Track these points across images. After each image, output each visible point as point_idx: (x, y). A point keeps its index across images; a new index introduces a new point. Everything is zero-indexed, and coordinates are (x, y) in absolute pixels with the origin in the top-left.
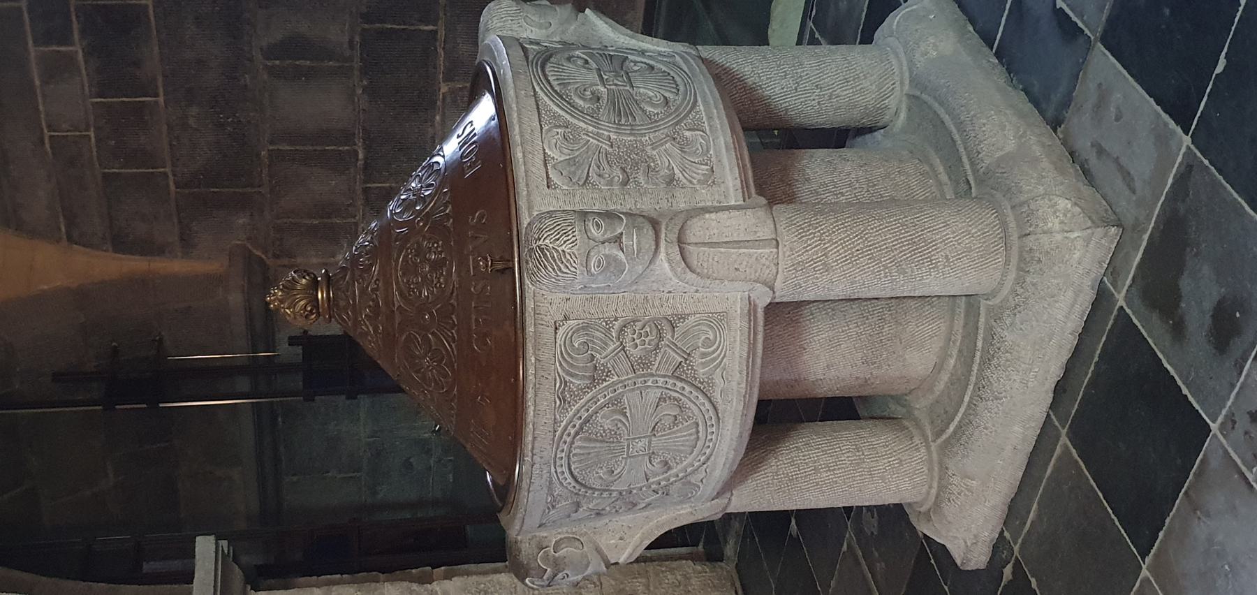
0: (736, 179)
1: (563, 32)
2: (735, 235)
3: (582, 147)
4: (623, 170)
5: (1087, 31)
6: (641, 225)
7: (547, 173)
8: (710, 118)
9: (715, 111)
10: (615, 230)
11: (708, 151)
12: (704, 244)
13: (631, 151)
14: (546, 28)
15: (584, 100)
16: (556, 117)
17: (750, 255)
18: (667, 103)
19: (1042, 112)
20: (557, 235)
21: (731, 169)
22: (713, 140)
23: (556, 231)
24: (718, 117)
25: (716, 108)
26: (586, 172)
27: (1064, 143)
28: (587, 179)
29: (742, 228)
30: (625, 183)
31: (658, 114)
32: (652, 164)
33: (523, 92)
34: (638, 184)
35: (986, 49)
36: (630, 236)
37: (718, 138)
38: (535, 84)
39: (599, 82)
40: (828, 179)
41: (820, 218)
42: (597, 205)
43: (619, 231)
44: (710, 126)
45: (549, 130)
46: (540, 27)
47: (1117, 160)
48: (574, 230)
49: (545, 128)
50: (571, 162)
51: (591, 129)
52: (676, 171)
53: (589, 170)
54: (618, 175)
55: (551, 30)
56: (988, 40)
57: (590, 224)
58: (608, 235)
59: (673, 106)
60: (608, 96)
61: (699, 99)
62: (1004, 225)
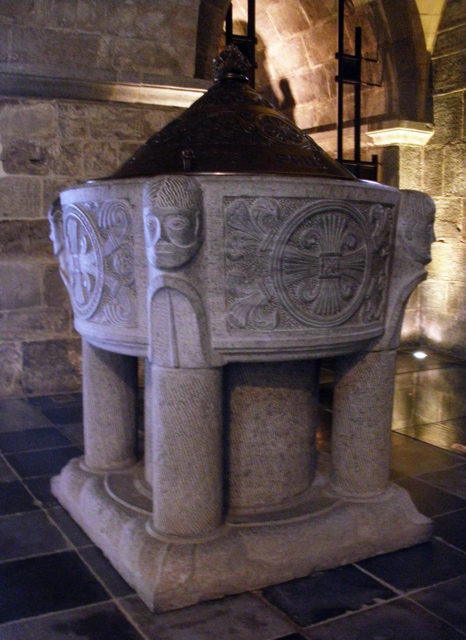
0: (233, 345)
1: (404, 249)
2: (182, 336)
3: (260, 227)
4: (241, 257)
5: (313, 626)
6: (177, 259)
7: (238, 197)
8: (290, 334)
9: (296, 339)
10: (173, 237)
11: (259, 327)
12: (172, 309)
13: (258, 267)
14: (407, 236)
15: (307, 236)
16: (289, 212)
17: (167, 345)
18: (306, 303)
19: (282, 584)
20: (168, 192)
21: (241, 342)
22: (268, 333)
23: (172, 192)
24: (289, 341)
25: (298, 340)
26: (238, 228)
27: (249, 593)
28: (233, 228)
29: (187, 342)
30: (228, 256)
31: (294, 293)
32: (247, 282)
33: (311, 189)
34: (230, 267)
35: (356, 559)
36: (167, 248)
37: (270, 336)
38: (321, 201)
39: (325, 252)
40: (269, 428)
41: (199, 405)
42: (211, 233)
43: (173, 240)
44: (281, 333)
45: (274, 204)
46: (408, 232)
47: (204, 622)
48: (172, 205)
49: (278, 202)
50: (247, 217)
51: (277, 237)
52: (241, 299)
53: (240, 230)
54: (236, 252)
55: (406, 240)
56: (361, 563)
57: (178, 219)
58: (169, 232)
59: (303, 308)
60: (311, 256)
61: (306, 329)
62: (186, 536)
